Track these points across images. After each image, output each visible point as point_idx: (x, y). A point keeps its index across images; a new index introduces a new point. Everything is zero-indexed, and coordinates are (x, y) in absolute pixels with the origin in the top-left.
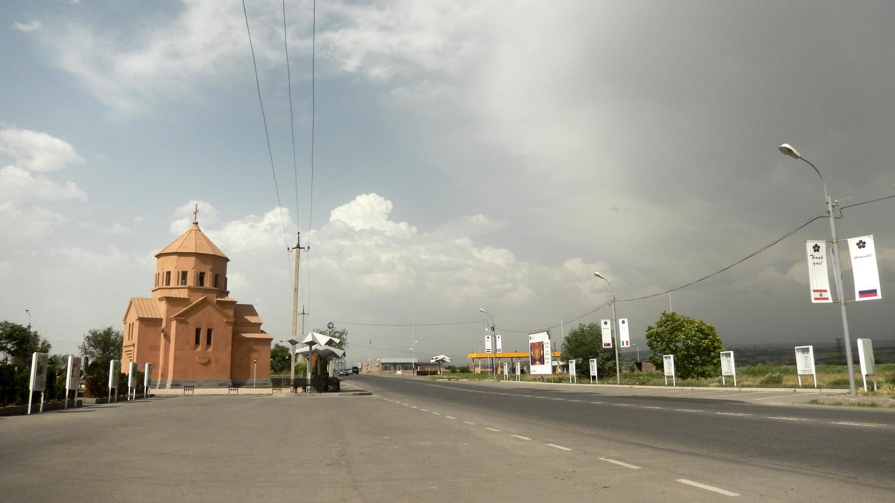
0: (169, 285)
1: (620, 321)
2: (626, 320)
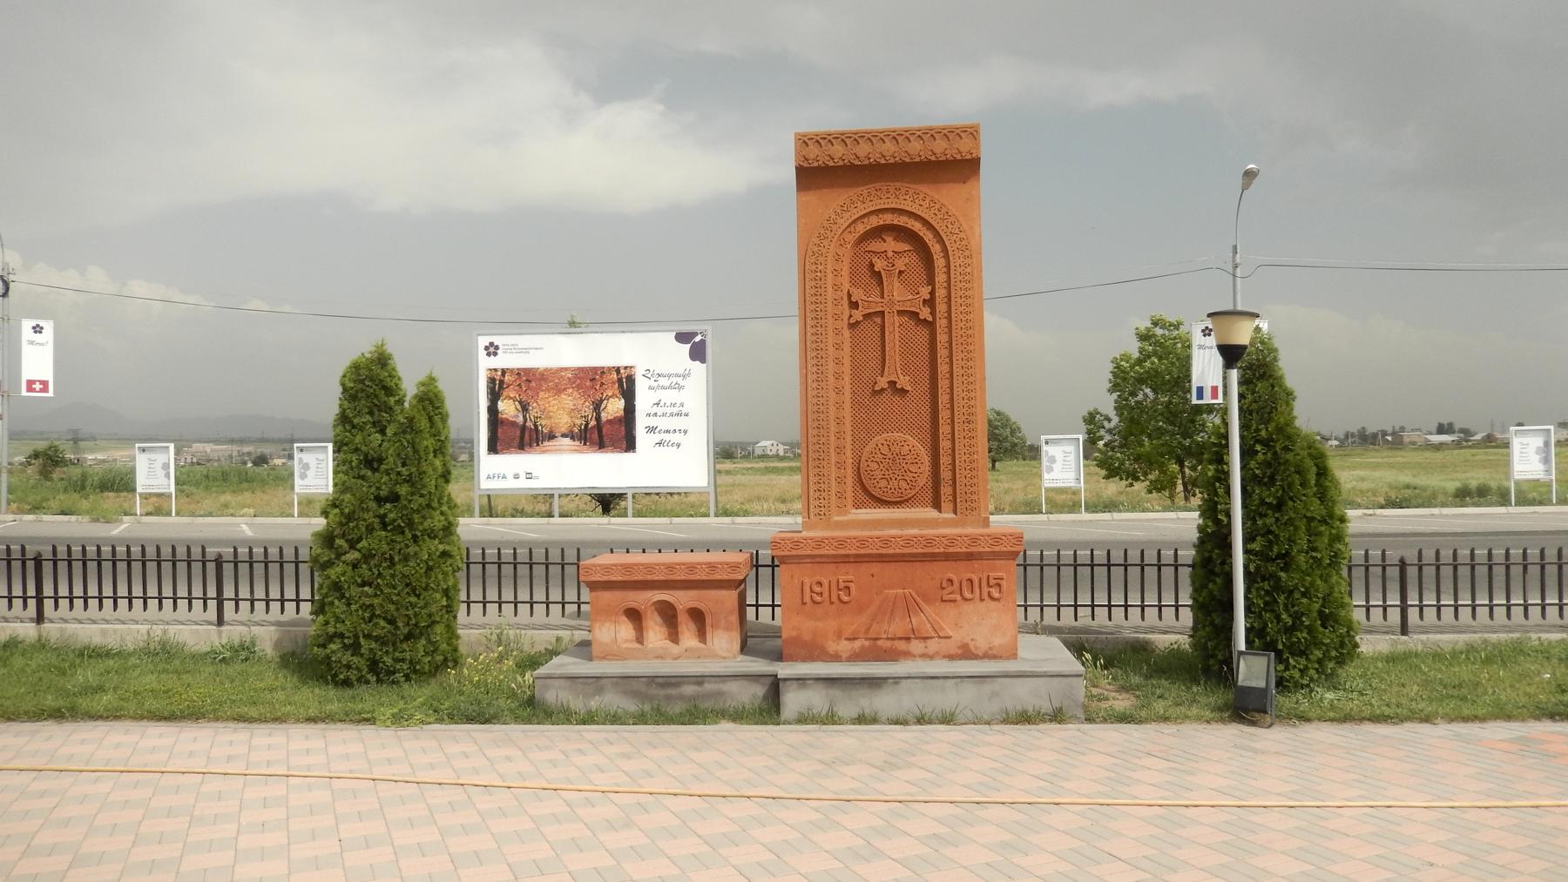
1: (27, 325)
2: (48, 327)
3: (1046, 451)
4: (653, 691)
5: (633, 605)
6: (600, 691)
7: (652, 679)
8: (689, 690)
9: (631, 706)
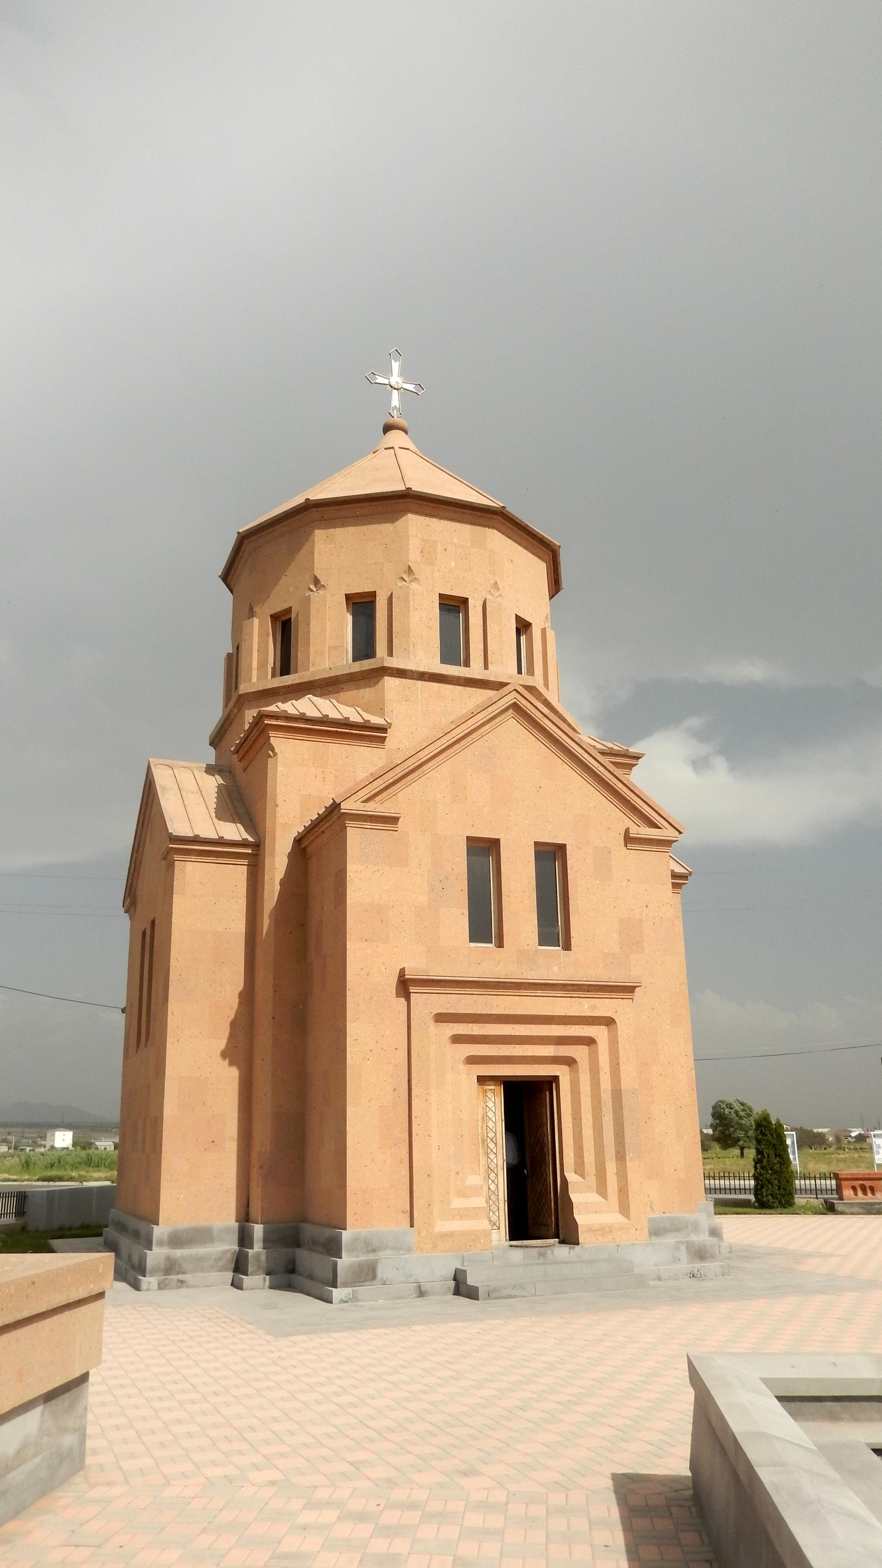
3: (243, 690)
4: (868, 1207)
5: (854, 1185)
6: (853, 1207)
7: (866, 1204)
8: (877, 1206)
9: (861, 1210)
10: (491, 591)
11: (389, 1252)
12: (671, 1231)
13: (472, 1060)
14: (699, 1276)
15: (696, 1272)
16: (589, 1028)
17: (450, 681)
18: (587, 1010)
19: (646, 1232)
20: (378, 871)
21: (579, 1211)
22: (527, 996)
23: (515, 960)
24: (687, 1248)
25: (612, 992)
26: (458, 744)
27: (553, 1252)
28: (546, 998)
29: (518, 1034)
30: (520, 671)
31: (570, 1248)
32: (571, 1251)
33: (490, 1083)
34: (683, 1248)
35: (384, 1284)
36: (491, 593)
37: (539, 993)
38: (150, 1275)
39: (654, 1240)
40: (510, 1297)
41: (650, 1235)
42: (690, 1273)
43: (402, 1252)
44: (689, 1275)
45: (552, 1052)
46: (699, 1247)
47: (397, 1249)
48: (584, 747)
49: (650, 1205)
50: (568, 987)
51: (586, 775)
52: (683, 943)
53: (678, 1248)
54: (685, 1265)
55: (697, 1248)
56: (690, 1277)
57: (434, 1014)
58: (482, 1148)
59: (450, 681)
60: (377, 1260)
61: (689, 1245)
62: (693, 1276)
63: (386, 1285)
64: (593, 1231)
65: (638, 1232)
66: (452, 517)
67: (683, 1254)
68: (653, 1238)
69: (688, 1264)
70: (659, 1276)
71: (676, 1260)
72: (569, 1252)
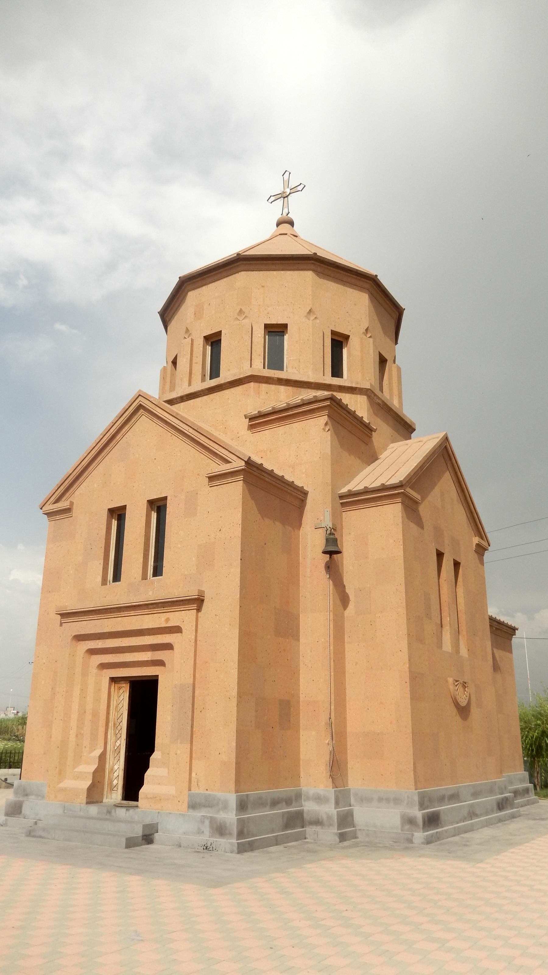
0: (215, 372)
10: (237, 318)
11: (33, 797)
12: (204, 806)
13: (103, 666)
14: (211, 849)
15: (209, 844)
16: (170, 636)
17: (199, 395)
18: (163, 623)
19: (185, 805)
20: (60, 545)
21: (148, 782)
22: (125, 616)
23: (126, 591)
24: (211, 822)
25: (180, 606)
26: (108, 447)
27: (115, 811)
28: (137, 616)
29: (124, 645)
30: (264, 368)
31: (127, 810)
32: (127, 812)
33: (122, 682)
34: (207, 822)
35: (25, 818)
36: (238, 319)
37: (132, 613)
38: (426, 819)
39: (192, 813)
40: (40, 837)
41: (189, 807)
42: (204, 845)
43: (40, 798)
44: (203, 847)
45: (150, 658)
46: (220, 824)
47: (37, 795)
48: (179, 418)
49: (197, 782)
50: (150, 606)
51: (185, 438)
52: (402, 547)
53: (202, 822)
54: (206, 837)
55: (219, 825)
56: (204, 849)
57: (73, 636)
58: (114, 730)
59: (199, 395)
60: (23, 801)
61: (212, 820)
62: (206, 849)
63: (26, 818)
64: (148, 798)
65: (180, 803)
66: (214, 280)
67: (207, 830)
68: (191, 810)
69: (209, 838)
70: (180, 843)
71: (200, 832)
72: (126, 813)
